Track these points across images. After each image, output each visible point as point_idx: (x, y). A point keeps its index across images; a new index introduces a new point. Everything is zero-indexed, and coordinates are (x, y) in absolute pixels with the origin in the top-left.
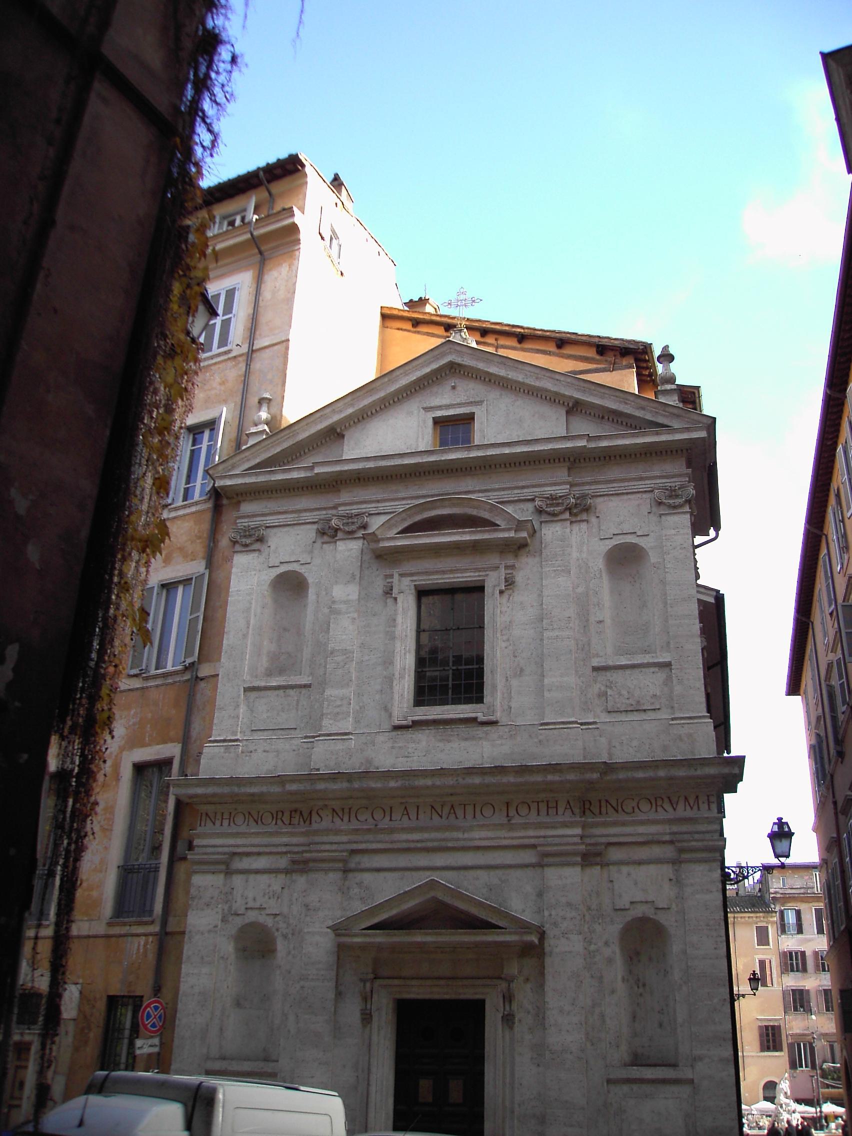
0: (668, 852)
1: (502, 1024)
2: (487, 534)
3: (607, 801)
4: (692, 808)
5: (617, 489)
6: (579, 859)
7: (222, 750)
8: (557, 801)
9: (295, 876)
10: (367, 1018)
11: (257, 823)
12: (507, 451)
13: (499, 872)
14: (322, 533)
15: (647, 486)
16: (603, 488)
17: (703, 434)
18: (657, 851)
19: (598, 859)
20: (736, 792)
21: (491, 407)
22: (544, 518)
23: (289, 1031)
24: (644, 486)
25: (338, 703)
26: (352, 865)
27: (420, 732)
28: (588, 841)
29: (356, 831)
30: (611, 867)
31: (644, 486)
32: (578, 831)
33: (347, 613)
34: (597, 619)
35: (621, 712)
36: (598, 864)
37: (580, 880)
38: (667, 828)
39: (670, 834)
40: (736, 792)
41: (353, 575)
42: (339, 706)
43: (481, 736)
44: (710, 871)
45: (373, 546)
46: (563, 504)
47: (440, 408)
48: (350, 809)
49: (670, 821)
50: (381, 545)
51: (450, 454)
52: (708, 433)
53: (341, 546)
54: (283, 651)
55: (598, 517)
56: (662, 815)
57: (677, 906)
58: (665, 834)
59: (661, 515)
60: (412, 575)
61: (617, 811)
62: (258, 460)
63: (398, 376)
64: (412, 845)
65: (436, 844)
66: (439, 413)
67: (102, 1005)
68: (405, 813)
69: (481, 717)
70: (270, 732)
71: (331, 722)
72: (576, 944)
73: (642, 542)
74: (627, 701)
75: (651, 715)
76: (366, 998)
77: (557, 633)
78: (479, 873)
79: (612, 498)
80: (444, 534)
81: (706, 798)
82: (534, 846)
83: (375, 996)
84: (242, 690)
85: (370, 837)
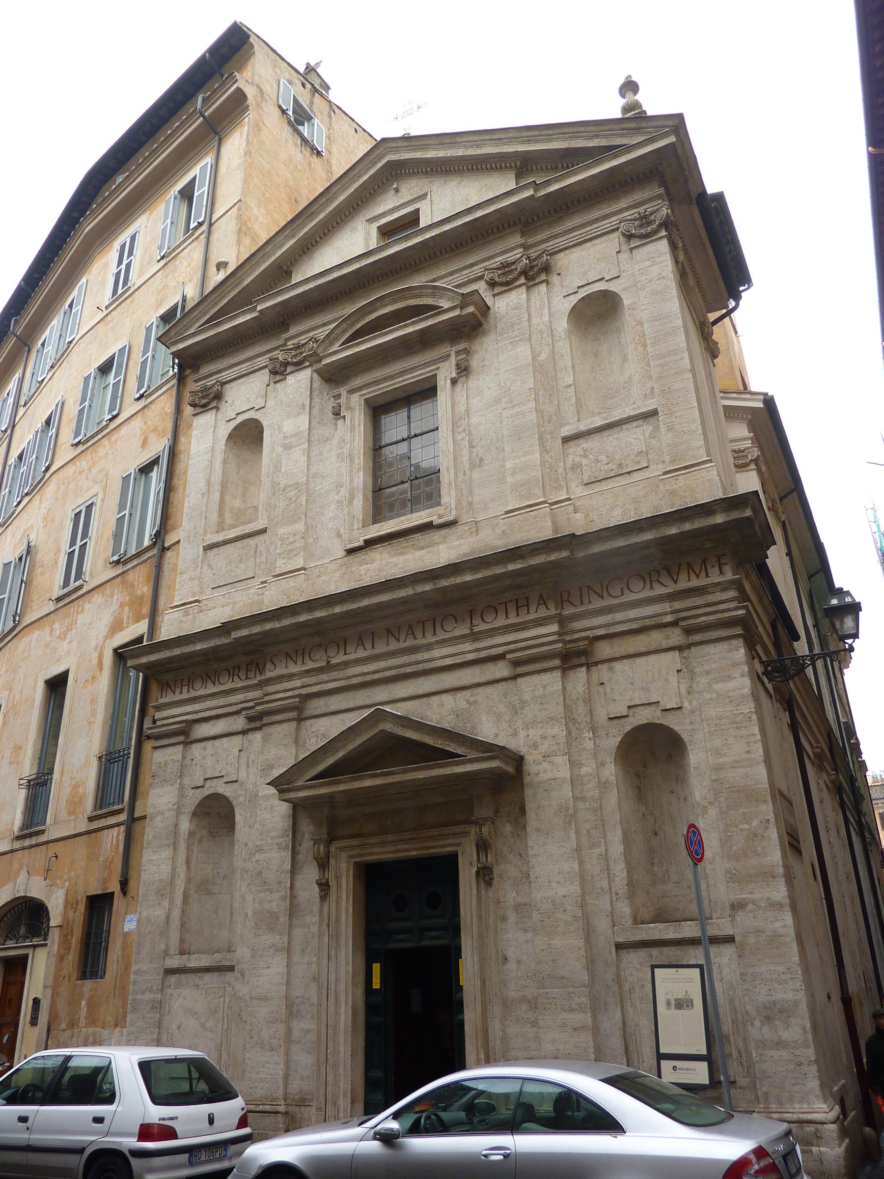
0: (676, 637)
1: (477, 882)
2: (431, 320)
3: (589, 587)
4: (698, 576)
5: (577, 237)
6: (557, 662)
7: (181, 613)
8: (527, 599)
9: (251, 736)
10: (324, 887)
11: (214, 685)
12: (447, 227)
13: (467, 694)
14: (274, 373)
15: (612, 224)
16: (561, 242)
17: (672, 139)
18: (657, 638)
19: (583, 660)
20: (680, 116)
21: (436, 197)
22: (497, 290)
23: (246, 914)
24: (609, 225)
25: (292, 539)
26: (307, 713)
27: (374, 551)
28: (568, 638)
29: (308, 672)
30: (600, 666)
31: (609, 225)
32: (554, 628)
33: (298, 445)
34: (566, 384)
35: (600, 481)
36: (581, 665)
37: (561, 687)
38: (667, 607)
39: (672, 612)
40: (680, 116)
41: (303, 406)
42: (291, 543)
43: (437, 541)
44: (730, 651)
45: (317, 366)
46: (516, 269)
47: (383, 215)
48: (303, 650)
49: (672, 597)
50: (323, 363)
51: (388, 250)
52: (678, 136)
53: (291, 379)
54: (249, 505)
55: (559, 274)
56: (660, 590)
57: (690, 703)
58: (665, 614)
59: (631, 249)
60: (360, 388)
61: (602, 597)
62: (207, 317)
63: (336, 193)
64: (368, 678)
65: (393, 672)
66: (383, 221)
67: (82, 908)
68: (410, 632)
69: (437, 521)
70: (229, 586)
71: (284, 561)
72: (560, 768)
73: (613, 287)
74: (606, 467)
75: (637, 476)
76: (323, 864)
77: (517, 409)
78: (445, 697)
79: (573, 250)
80: (386, 334)
81: (716, 559)
82: (501, 657)
83: (332, 862)
84: (201, 549)
85: (324, 677)
